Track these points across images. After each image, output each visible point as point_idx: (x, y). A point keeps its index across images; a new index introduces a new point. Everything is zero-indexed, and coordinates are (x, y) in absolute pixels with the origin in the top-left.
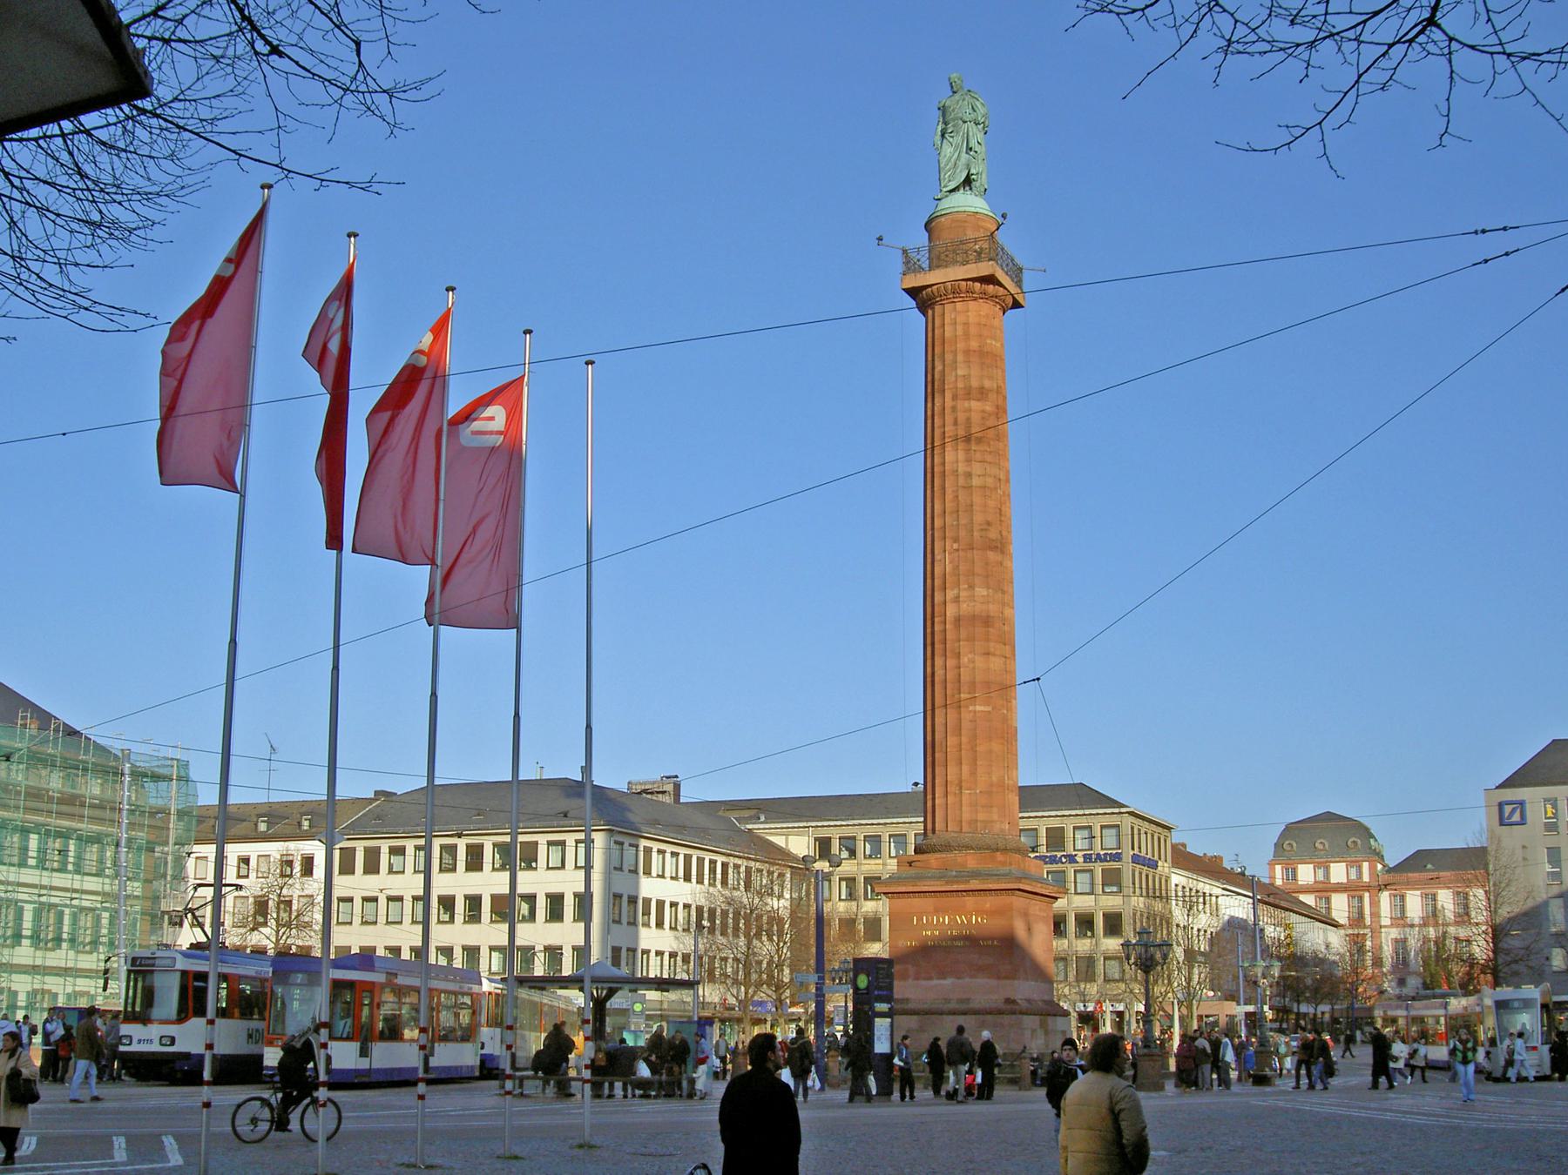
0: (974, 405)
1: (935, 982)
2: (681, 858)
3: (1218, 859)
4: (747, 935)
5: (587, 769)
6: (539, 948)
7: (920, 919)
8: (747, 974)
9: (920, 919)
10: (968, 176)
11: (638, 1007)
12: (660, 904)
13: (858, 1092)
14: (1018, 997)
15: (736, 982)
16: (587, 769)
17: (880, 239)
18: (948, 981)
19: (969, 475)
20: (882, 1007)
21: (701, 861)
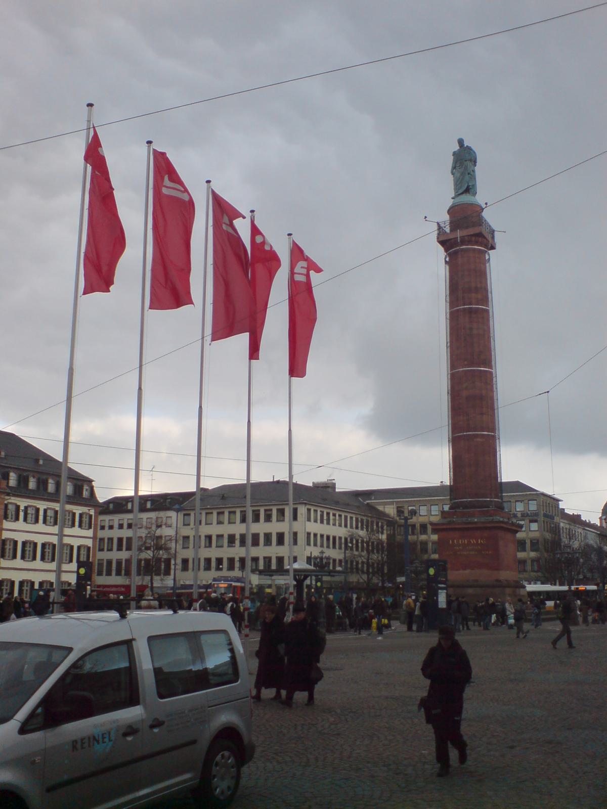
0: (473, 295)
1: (461, 572)
2: (343, 517)
3: (579, 516)
4: (368, 550)
5: (291, 476)
6: (237, 559)
7: (453, 542)
8: (368, 569)
9: (453, 542)
10: (468, 186)
11: (576, 577)
12: (315, 535)
13: (410, 629)
14: (502, 578)
15: (363, 572)
16: (291, 476)
17: (426, 217)
18: (467, 571)
19: (471, 329)
20: (89, 583)
21: (346, 517)
